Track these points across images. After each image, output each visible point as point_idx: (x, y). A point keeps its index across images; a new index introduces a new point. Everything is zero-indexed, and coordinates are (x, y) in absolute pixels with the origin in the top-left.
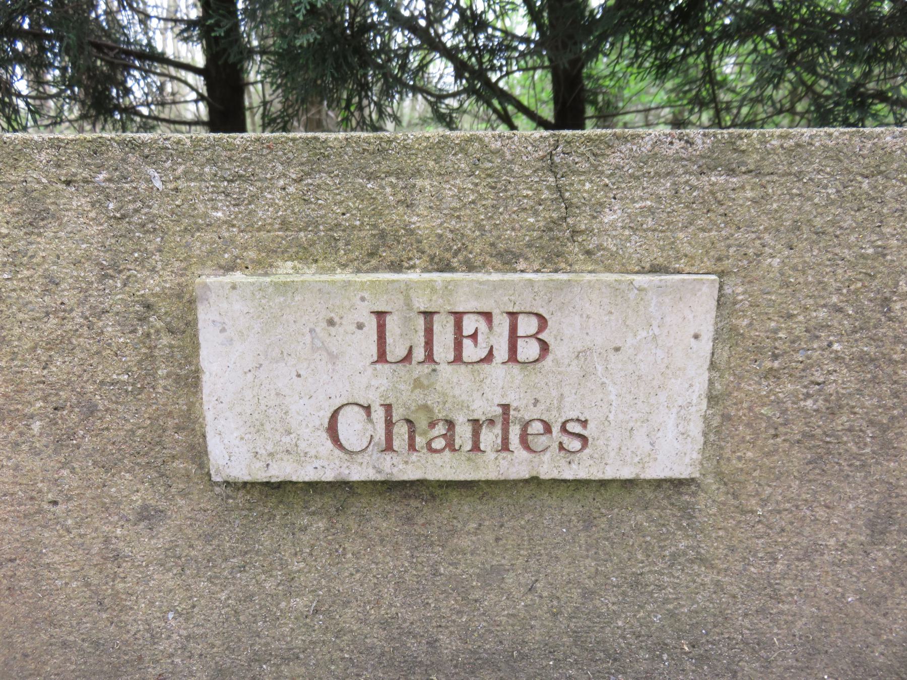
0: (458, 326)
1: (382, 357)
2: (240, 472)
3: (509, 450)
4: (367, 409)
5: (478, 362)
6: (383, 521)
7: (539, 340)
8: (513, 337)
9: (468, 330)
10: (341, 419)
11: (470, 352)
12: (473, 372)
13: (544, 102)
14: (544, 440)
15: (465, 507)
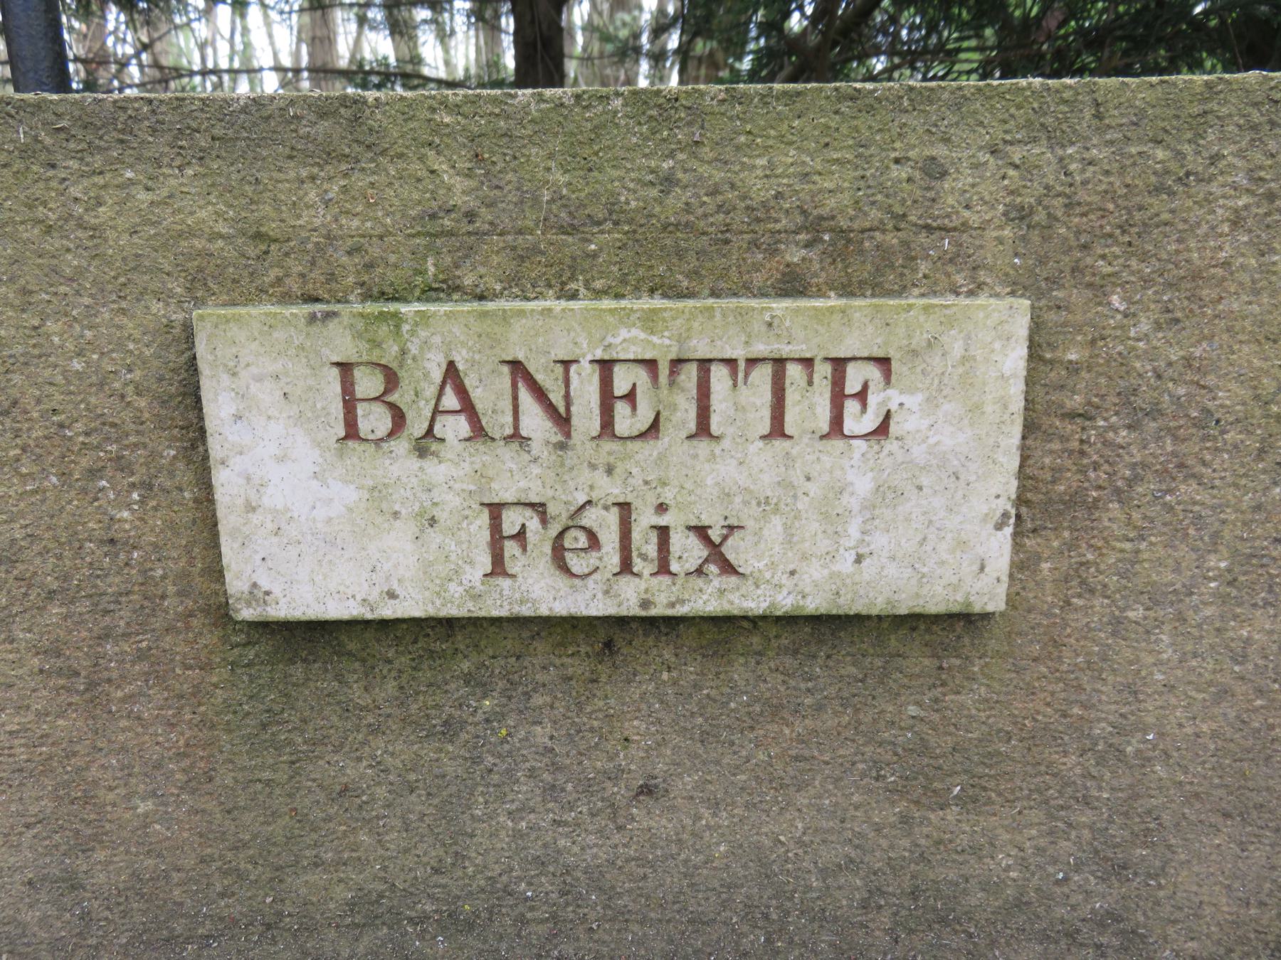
0: (838, 382)
1: (352, 431)
3: (710, 435)
9: (621, 387)
11: (625, 421)
14: (592, 559)
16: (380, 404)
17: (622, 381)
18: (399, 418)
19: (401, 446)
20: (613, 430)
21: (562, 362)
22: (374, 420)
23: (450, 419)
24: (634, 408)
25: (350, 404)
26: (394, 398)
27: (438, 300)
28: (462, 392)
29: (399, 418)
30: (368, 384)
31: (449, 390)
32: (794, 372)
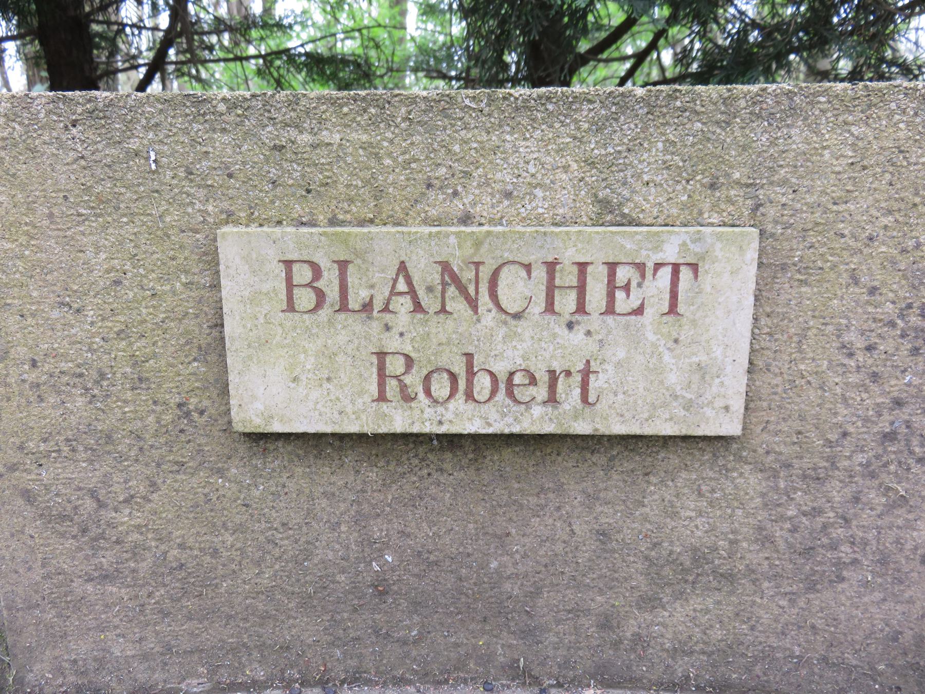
0: (612, 275)
1: (291, 307)
2: (258, 424)
4: (528, 268)
5: (630, 314)
6: (454, 474)
7: (314, 288)
8: (581, 289)
10: (505, 270)
11: (622, 302)
12: (627, 327)
13: (129, 79)
14: (532, 390)
15: (565, 466)
16: (309, 290)
17: (623, 274)
18: (321, 296)
19: (324, 313)
20: (584, 307)
21: (474, 263)
22: (566, 302)
23: (401, 299)
24: (628, 295)
25: (551, 289)
26: (319, 284)
27: (345, 226)
28: (409, 282)
29: (321, 296)
30: (303, 274)
31: (401, 280)
32: (685, 274)
